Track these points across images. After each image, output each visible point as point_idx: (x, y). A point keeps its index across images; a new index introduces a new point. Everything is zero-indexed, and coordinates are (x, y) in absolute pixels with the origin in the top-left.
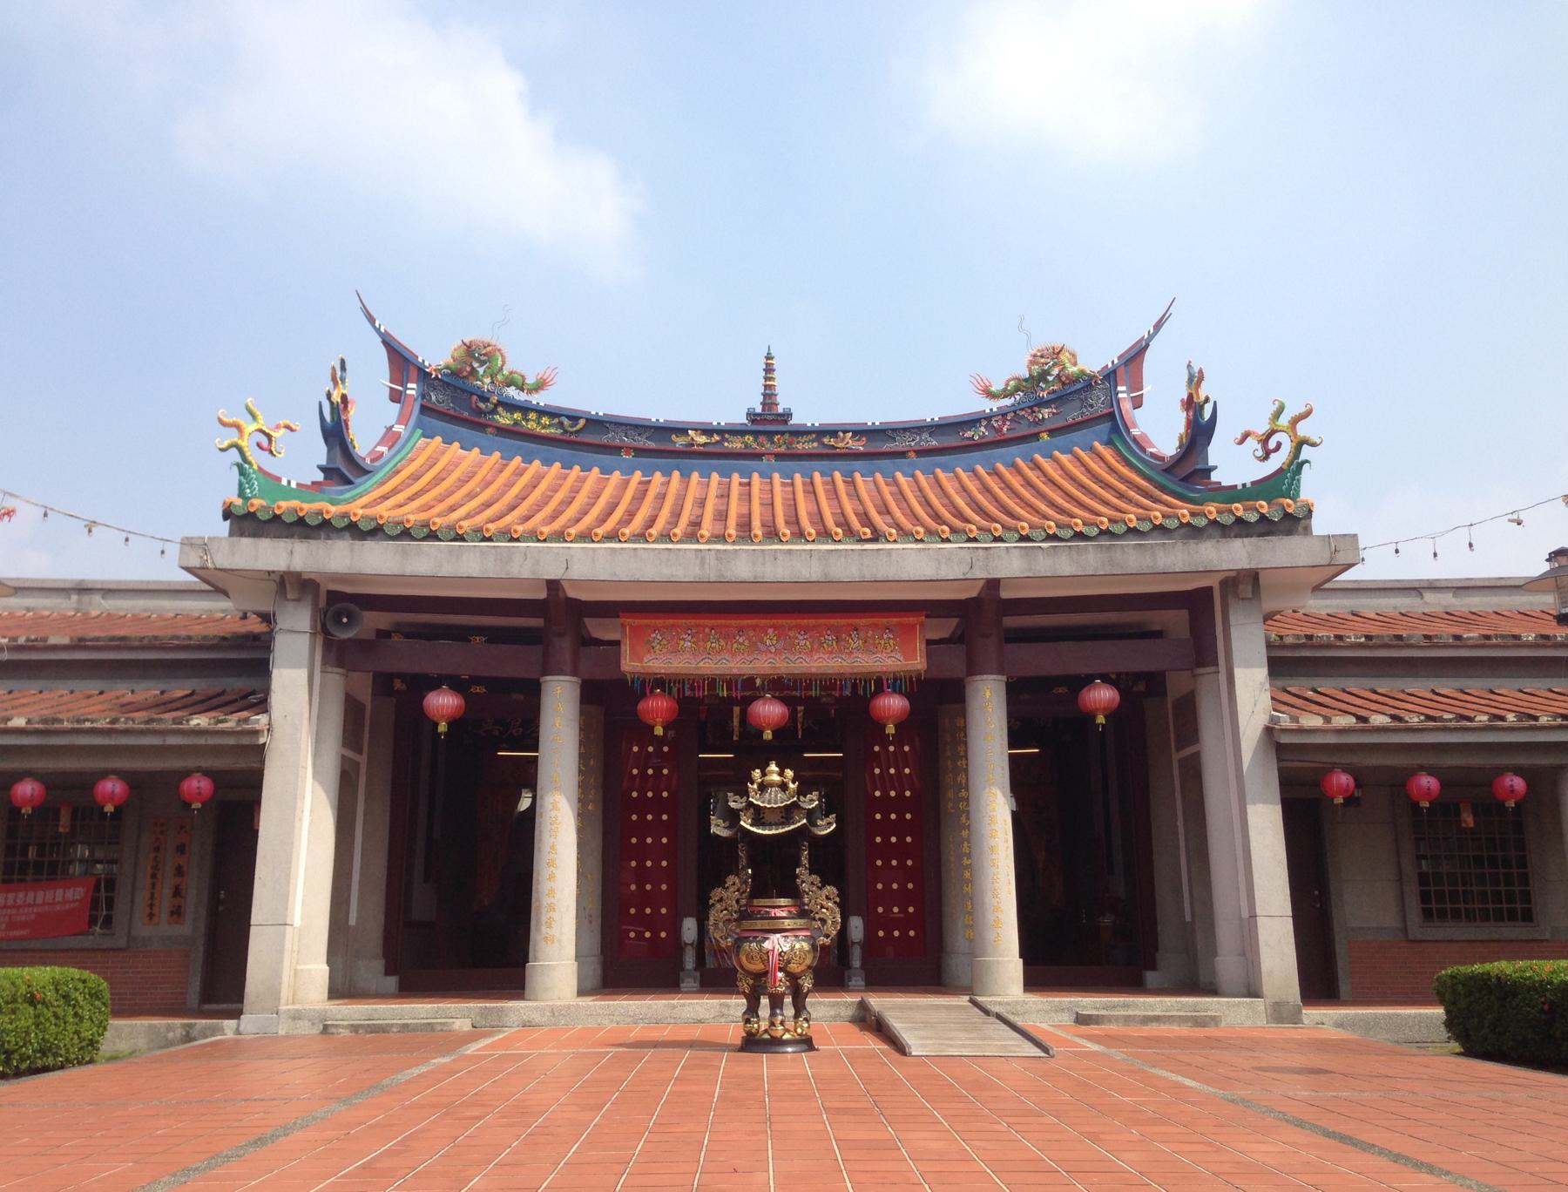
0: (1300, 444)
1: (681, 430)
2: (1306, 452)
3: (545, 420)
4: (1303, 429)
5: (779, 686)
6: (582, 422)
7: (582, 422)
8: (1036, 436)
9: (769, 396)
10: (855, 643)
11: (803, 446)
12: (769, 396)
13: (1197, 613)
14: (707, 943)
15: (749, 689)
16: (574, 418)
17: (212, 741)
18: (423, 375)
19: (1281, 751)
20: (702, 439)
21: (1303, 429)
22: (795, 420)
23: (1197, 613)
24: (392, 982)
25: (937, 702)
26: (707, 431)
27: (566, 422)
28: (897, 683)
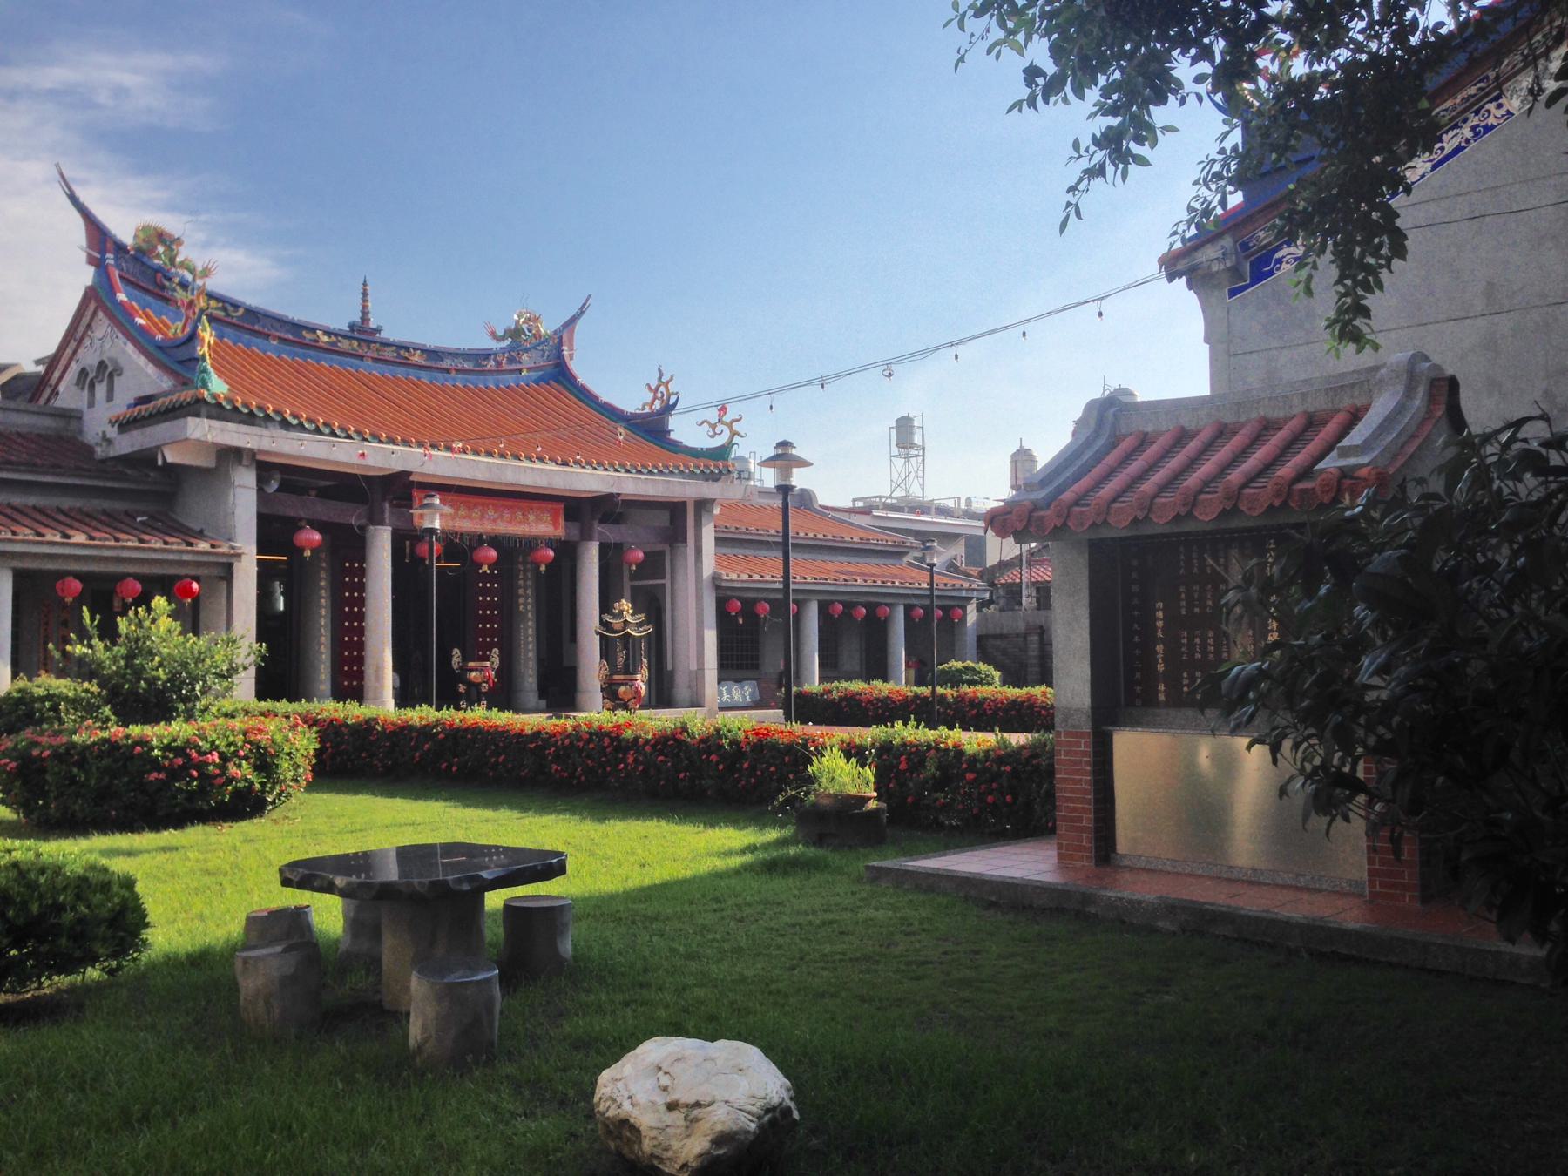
0: (734, 434)
1: (313, 330)
2: (736, 439)
3: (213, 303)
4: (736, 426)
5: (495, 541)
6: (241, 311)
7: (241, 311)
8: (520, 371)
9: (365, 313)
10: (532, 517)
11: (389, 354)
12: (365, 313)
13: (674, 519)
14: (190, 620)
15: (478, 540)
16: (236, 306)
17: (211, 559)
18: (120, 248)
19: (718, 588)
20: (325, 339)
21: (736, 426)
22: (384, 335)
23: (674, 519)
24: (543, 703)
25: (568, 553)
26: (328, 333)
27: (230, 308)
28: (550, 543)
